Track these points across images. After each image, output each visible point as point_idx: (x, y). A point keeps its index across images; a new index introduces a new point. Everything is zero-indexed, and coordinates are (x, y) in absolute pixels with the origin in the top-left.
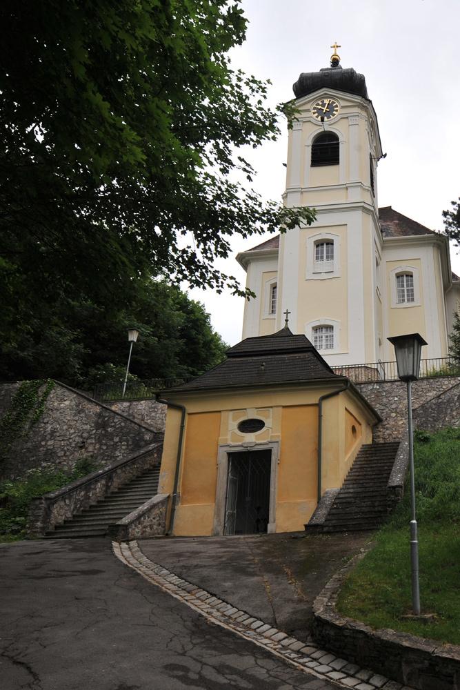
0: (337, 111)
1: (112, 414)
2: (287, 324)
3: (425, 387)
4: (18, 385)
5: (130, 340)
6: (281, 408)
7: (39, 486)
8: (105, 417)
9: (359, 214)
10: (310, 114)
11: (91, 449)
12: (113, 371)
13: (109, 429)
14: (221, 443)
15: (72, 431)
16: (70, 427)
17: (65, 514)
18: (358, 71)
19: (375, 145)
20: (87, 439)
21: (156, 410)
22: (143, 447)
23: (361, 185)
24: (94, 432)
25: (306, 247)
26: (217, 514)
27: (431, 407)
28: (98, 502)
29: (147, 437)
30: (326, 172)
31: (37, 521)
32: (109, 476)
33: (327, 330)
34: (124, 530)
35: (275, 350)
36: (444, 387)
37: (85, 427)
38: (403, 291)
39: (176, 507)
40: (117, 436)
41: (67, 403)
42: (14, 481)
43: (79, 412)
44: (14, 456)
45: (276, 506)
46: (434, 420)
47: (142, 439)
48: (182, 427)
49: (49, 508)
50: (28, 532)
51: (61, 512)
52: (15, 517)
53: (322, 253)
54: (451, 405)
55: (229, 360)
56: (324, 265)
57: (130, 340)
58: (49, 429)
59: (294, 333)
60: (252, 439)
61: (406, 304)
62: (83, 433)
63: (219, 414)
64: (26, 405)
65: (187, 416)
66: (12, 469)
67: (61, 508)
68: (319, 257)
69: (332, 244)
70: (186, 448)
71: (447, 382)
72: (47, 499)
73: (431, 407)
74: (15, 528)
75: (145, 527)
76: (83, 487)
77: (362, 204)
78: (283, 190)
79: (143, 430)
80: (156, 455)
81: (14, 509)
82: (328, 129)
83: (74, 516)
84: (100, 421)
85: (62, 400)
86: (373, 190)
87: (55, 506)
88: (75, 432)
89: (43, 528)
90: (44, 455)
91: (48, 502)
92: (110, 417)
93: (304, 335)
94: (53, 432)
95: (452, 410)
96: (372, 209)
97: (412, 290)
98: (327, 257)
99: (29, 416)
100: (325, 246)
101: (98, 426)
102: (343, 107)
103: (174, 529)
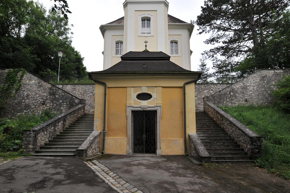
1: (57, 89)
2: (146, 48)
3: (202, 88)
4: (7, 71)
5: (59, 56)
6: (161, 88)
7: (25, 122)
8: (54, 90)
11: (48, 105)
12: (50, 73)
13: (57, 96)
14: (128, 105)
15: (37, 96)
16: (36, 94)
17: (45, 140)
20: (46, 100)
21: (75, 90)
22: (75, 106)
24: (49, 97)
25: (138, 20)
26: (128, 143)
27: (216, 96)
28: (61, 133)
29: (77, 101)
31: (30, 144)
32: (64, 119)
34: (85, 153)
35: (149, 57)
37: (44, 94)
38: (173, 49)
39: (105, 138)
40: (61, 100)
41: (33, 81)
42: (11, 118)
43: (40, 86)
44: (9, 107)
45: (161, 141)
46: (218, 103)
47: (74, 102)
48: (105, 94)
49: (35, 136)
50: (25, 151)
51: (43, 139)
52: (14, 140)
53: (145, 24)
54: (226, 96)
55: (123, 61)
56: (146, 30)
57: (59, 56)
58: (25, 94)
60: (145, 104)
62: (43, 97)
63: (125, 89)
64: (11, 80)
65: (107, 89)
66: (9, 113)
67: (42, 136)
68: (143, 26)
70: (108, 106)
71: (213, 86)
72: (34, 131)
73: (216, 96)
74: (15, 147)
75: (93, 150)
76: (52, 125)
79: (74, 98)
80: (82, 110)
81: (13, 135)
83: (50, 141)
84: (51, 91)
85: (30, 80)
87: (39, 135)
88: (39, 97)
89: (33, 149)
90: (24, 107)
91: (35, 133)
92: (56, 90)
93: (161, 52)
94: (28, 96)
95: (227, 98)
98: (147, 26)
99: (14, 87)
101: (50, 94)
103: (105, 150)
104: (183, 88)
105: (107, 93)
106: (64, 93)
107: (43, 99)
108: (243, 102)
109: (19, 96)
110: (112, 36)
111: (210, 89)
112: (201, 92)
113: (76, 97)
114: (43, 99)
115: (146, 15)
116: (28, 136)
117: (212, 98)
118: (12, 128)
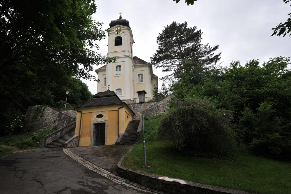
4: (37, 106)
9: (128, 58)
10: (114, 32)
11: (57, 123)
15: (51, 119)
16: (51, 117)
26: (91, 140)
29: (72, 120)
30: (119, 48)
32: (62, 130)
38: (140, 79)
39: (80, 139)
42: (36, 132)
48: (81, 117)
51: (49, 141)
53: (118, 69)
56: (119, 72)
59: (111, 91)
60: (100, 120)
61: (141, 83)
64: (38, 111)
65: (82, 114)
68: (117, 70)
72: (45, 137)
73: (148, 110)
74: (37, 145)
78: (107, 53)
81: (36, 140)
82: (119, 35)
84: (59, 116)
85: (49, 110)
92: (61, 115)
94: (46, 119)
98: (119, 70)
99: (40, 115)
101: (58, 117)
102: (123, 30)
104: (118, 110)
105: (82, 116)
106: (66, 116)
107: (54, 120)
108: (163, 112)
109: (42, 119)
112: (146, 107)
113: (72, 118)
114: (54, 120)
116: (43, 139)
118: (36, 137)
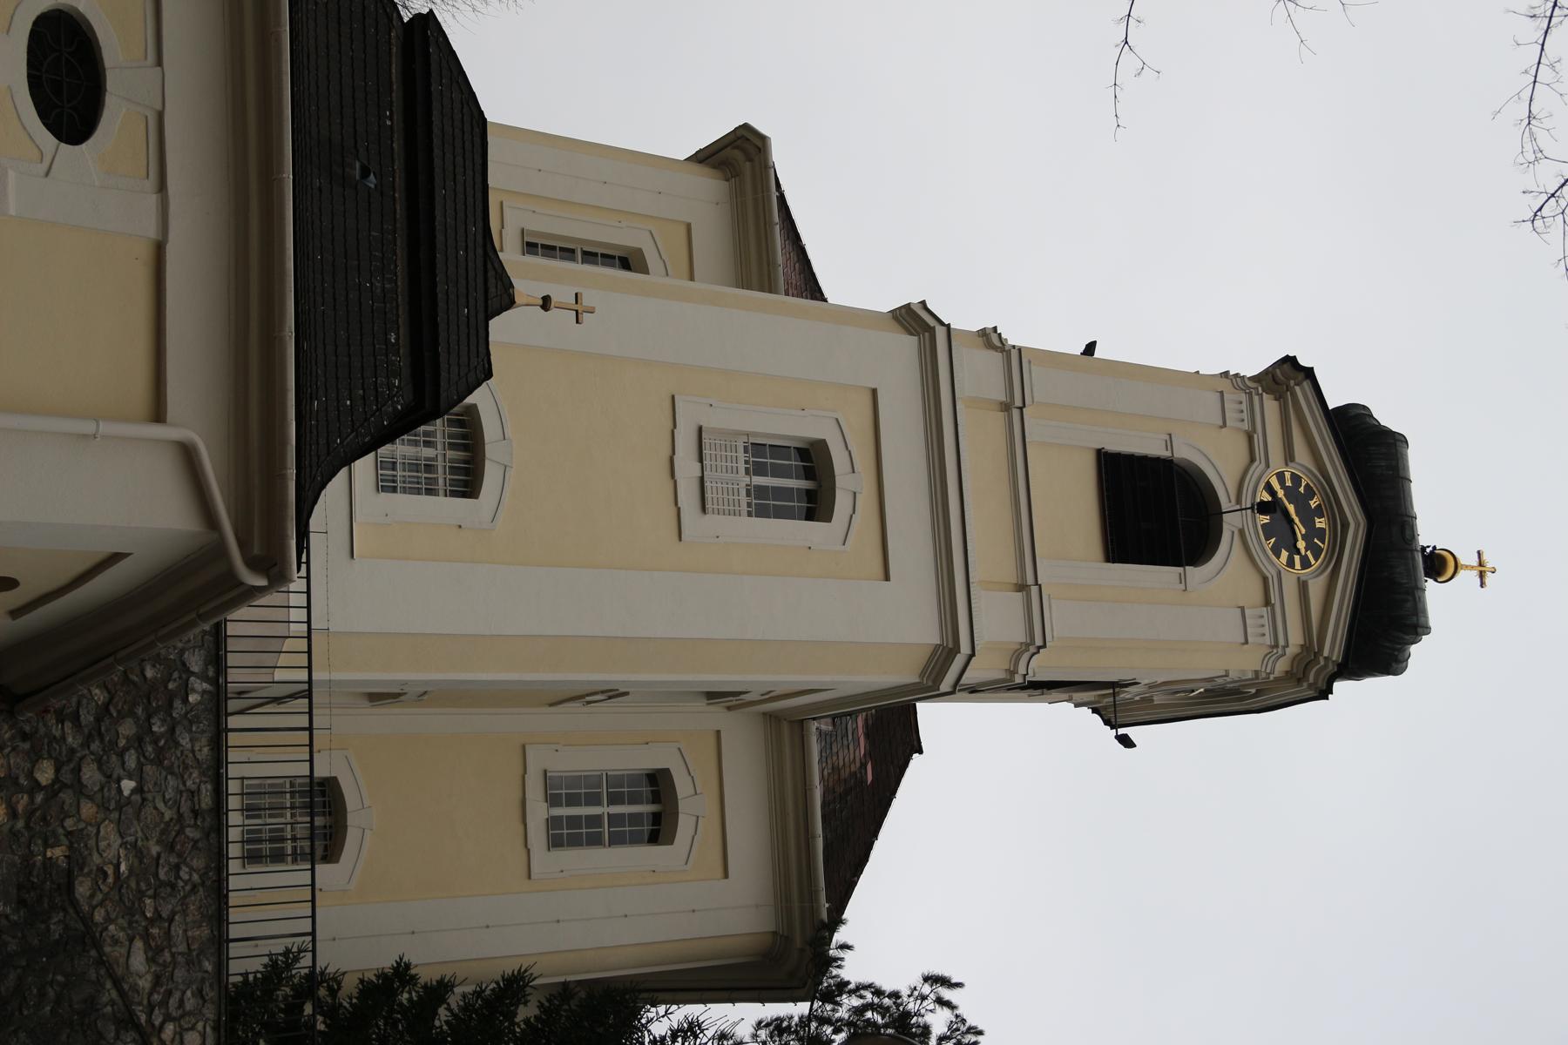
0: (1291, 563)
3: (177, 930)
6: (152, 232)
9: (927, 634)
10: (1277, 464)
18: (1418, 652)
19: (1158, 699)
23: (1033, 645)
30: (1070, 508)
33: (453, 470)
36: (170, 1028)
38: (594, 800)
53: (778, 472)
59: (494, 324)
61: (539, 811)
68: (762, 455)
69: (810, 516)
77: (965, 648)
78: (1013, 338)
82: (1230, 523)
86: (1010, 689)
93: (488, 374)
96: (945, 686)
97: (595, 841)
98: (761, 492)
100: (803, 484)
102: (1303, 587)
110: (689, 227)
111: (168, 1018)
115: (850, 482)
117: (56, 931)
